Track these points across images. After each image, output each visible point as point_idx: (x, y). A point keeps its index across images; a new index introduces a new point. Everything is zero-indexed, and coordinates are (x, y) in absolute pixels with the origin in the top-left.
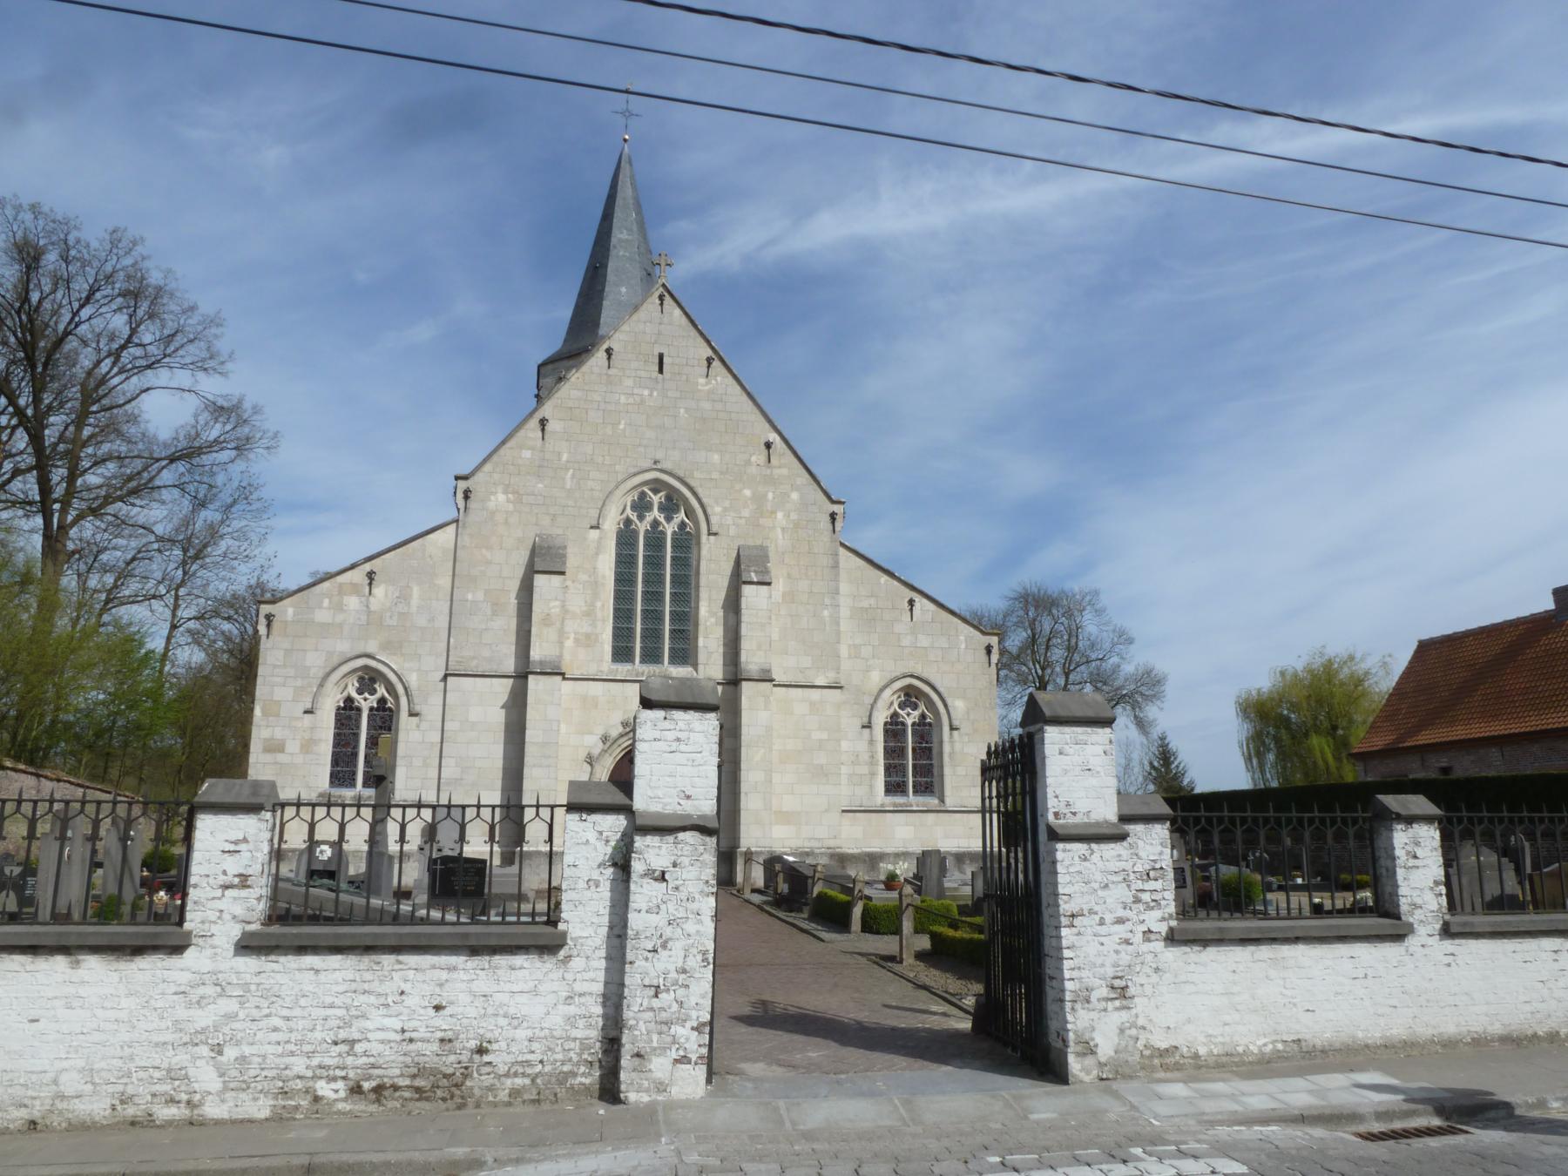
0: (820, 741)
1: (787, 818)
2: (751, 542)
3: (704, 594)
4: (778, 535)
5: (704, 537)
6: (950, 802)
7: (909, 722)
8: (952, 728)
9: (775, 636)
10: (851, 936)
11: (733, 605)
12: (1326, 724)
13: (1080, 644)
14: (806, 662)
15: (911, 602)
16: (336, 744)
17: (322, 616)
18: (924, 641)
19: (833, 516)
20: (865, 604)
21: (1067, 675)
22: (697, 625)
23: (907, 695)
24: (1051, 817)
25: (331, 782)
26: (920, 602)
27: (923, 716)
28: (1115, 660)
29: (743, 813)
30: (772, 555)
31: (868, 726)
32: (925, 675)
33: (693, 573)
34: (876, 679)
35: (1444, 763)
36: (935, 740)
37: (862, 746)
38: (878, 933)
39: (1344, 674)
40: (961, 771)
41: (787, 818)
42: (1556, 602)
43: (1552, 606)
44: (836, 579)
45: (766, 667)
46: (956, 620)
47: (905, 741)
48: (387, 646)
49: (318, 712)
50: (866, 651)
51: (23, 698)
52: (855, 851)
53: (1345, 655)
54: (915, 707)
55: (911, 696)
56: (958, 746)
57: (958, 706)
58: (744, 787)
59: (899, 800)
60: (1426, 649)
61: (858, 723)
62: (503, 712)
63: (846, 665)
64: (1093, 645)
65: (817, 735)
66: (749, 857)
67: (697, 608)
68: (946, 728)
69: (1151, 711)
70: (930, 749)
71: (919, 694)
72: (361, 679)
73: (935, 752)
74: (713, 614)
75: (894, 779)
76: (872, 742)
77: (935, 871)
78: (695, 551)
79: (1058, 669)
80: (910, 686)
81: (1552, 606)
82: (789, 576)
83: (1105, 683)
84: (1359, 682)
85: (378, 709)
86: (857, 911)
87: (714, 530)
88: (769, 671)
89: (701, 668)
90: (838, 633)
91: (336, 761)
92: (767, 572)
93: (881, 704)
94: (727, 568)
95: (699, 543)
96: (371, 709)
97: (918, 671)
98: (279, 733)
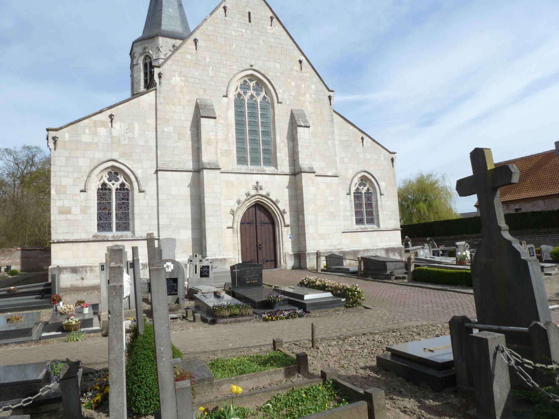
0: (331, 201)
5: (276, 104)
6: (382, 227)
7: (114, 188)
8: (381, 194)
11: (293, 138)
15: (362, 138)
16: (99, 209)
17: (86, 138)
18: (368, 156)
20: (344, 139)
25: (98, 229)
26: (366, 139)
27: (368, 189)
34: (351, 173)
35: (517, 207)
36: (373, 199)
42: (556, 147)
44: (333, 126)
46: (379, 147)
48: (124, 155)
49: (88, 191)
50: (346, 160)
52: (348, 250)
54: (365, 186)
56: (383, 202)
62: (189, 188)
68: (379, 195)
70: (371, 204)
72: (110, 173)
73: (374, 205)
80: (364, 176)
87: (280, 101)
89: (279, 167)
91: (100, 218)
93: (353, 184)
96: (117, 189)
98: (67, 203)
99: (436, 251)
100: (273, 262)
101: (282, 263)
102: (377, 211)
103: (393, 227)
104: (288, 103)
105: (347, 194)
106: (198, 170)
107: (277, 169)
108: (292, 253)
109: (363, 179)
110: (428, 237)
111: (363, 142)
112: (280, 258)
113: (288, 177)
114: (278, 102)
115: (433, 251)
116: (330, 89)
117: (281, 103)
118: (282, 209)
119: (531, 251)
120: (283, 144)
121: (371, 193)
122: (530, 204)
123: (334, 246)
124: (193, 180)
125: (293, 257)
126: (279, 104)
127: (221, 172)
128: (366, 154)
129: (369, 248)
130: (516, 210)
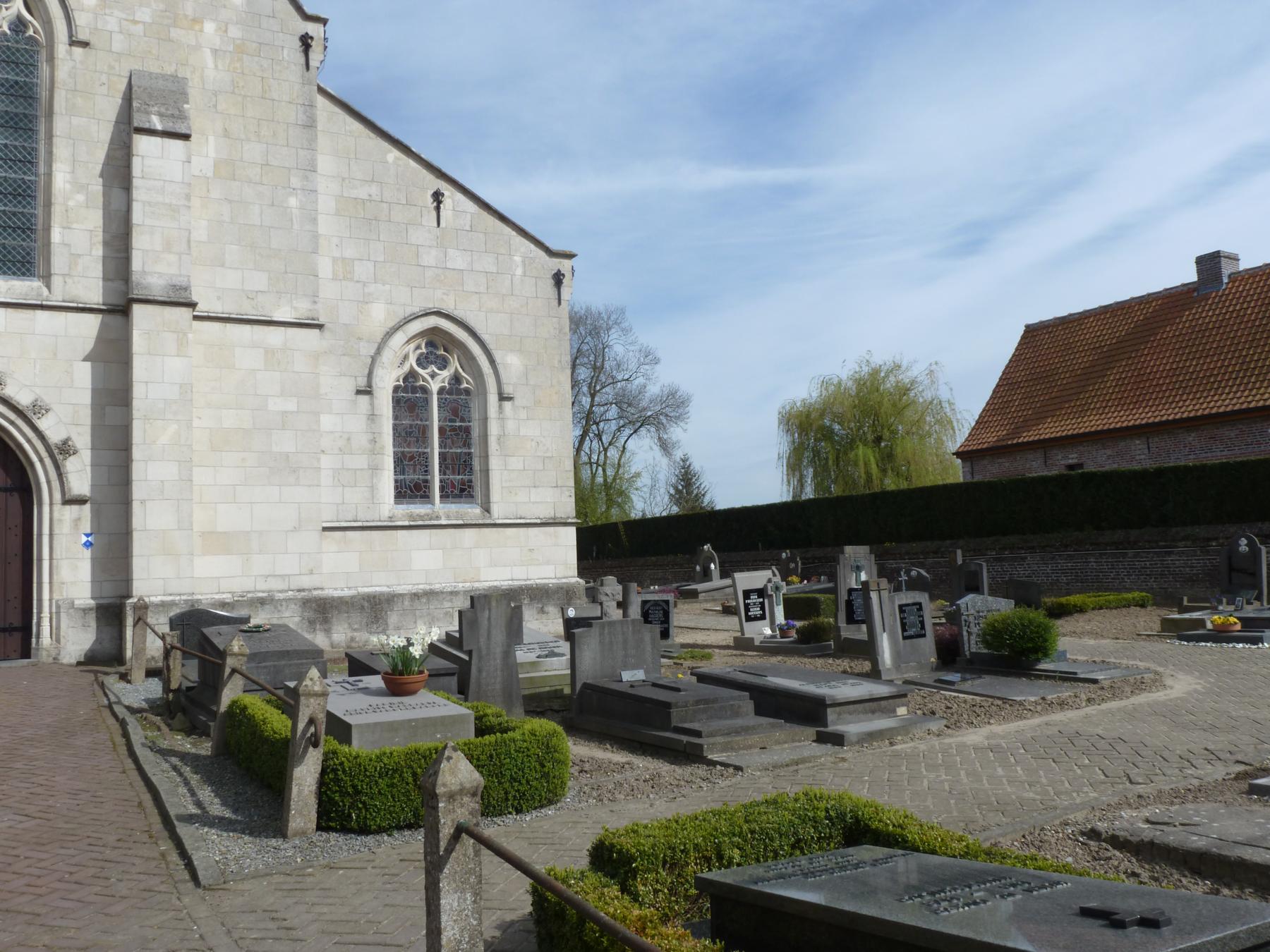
0: (284, 413)
1: (219, 542)
2: (153, 67)
3: (61, 150)
4: (205, 60)
5: (61, 48)
6: (499, 511)
7: (435, 386)
8: (503, 398)
9: (200, 234)
10: (287, 848)
11: (119, 173)
12: (870, 437)
13: (607, 365)
14: (258, 281)
15: (437, 197)
18: (458, 260)
19: (306, 41)
20: (362, 193)
21: (593, 396)
22: (48, 205)
23: (430, 344)
24: (437, 565)
26: (452, 198)
27: (456, 379)
28: (640, 380)
29: (136, 536)
30: (194, 92)
31: (367, 391)
32: (459, 314)
33: (41, 112)
34: (379, 316)
35: (1073, 459)
36: (475, 415)
37: (357, 425)
38: (364, 831)
39: (890, 383)
40: (515, 463)
41: (219, 542)
42: (1199, 272)
43: (1195, 279)
44: (311, 145)
45: (182, 281)
46: (508, 230)
47: (429, 418)
50: (363, 270)
51: (1022, 638)
52: (347, 593)
53: (890, 364)
54: (443, 365)
55: (437, 346)
56: (511, 425)
57: (511, 363)
58: (138, 491)
59: (419, 509)
60: (1033, 334)
61: (349, 385)
63: (328, 291)
64: (619, 365)
65: (276, 405)
66: (142, 609)
67: (49, 175)
68: (493, 398)
69: (675, 433)
70: (467, 430)
71: (452, 343)
73: (475, 433)
74: (79, 187)
75: (411, 477)
76: (372, 417)
77: (499, 637)
78: (44, 69)
79: (585, 389)
80: (435, 330)
81: (1195, 279)
82: (226, 133)
83: (630, 405)
84: (904, 390)
85: (405, 390)
86: (305, 776)
87: (82, 36)
88: (186, 289)
89: (56, 281)
90: (315, 237)
91: (401, 462)
92: (182, 117)
93: (388, 356)
94: (110, 108)
95: (51, 59)
97: (448, 307)
99: (656, 603)
100: (17, 636)
101: (46, 639)
102: (485, 457)
103: (545, 512)
104: (116, 46)
105: (359, 392)
106: (119, 309)
107: (48, 287)
108: (92, 603)
109: (438, 340)
110: (784, 548)
111: (438, 209)
112: (39, 618)
113: (94, 321)
114: (74, 42)
115: (644, 603)
116: (309, 10)
117: (85, 44)
118: (55, 437)
119: (912, 619)
120: (81, 198)
121: (467, 392)
122: (1109, 452)
123: (282, 576)
124: (101, 339)
125: (93, 615)
126: (78, 51)
127: (196, 318)
128: (451, 252)
129: (437, 587)
130: (1071, 467)
